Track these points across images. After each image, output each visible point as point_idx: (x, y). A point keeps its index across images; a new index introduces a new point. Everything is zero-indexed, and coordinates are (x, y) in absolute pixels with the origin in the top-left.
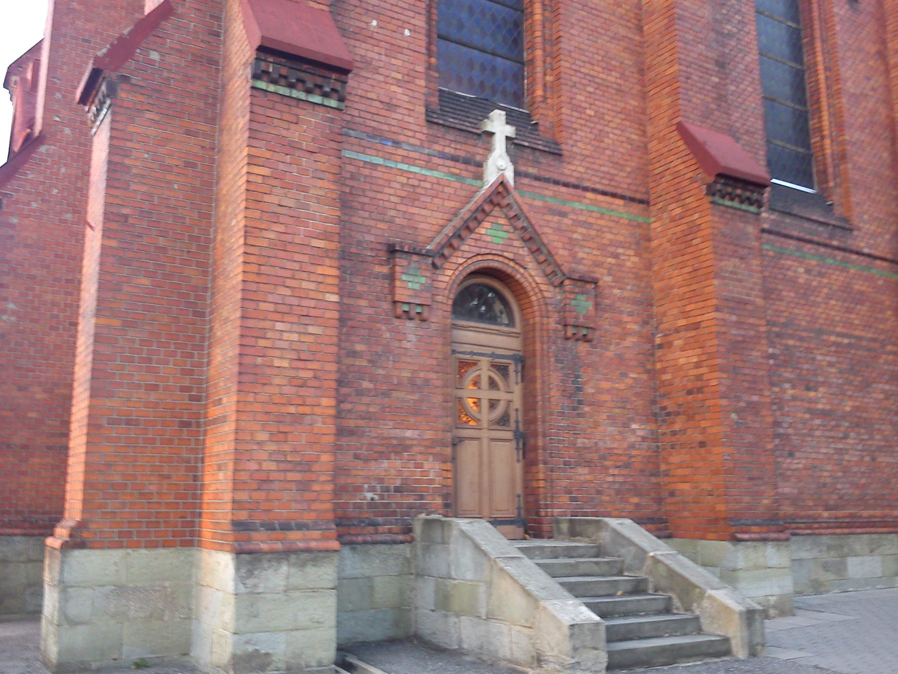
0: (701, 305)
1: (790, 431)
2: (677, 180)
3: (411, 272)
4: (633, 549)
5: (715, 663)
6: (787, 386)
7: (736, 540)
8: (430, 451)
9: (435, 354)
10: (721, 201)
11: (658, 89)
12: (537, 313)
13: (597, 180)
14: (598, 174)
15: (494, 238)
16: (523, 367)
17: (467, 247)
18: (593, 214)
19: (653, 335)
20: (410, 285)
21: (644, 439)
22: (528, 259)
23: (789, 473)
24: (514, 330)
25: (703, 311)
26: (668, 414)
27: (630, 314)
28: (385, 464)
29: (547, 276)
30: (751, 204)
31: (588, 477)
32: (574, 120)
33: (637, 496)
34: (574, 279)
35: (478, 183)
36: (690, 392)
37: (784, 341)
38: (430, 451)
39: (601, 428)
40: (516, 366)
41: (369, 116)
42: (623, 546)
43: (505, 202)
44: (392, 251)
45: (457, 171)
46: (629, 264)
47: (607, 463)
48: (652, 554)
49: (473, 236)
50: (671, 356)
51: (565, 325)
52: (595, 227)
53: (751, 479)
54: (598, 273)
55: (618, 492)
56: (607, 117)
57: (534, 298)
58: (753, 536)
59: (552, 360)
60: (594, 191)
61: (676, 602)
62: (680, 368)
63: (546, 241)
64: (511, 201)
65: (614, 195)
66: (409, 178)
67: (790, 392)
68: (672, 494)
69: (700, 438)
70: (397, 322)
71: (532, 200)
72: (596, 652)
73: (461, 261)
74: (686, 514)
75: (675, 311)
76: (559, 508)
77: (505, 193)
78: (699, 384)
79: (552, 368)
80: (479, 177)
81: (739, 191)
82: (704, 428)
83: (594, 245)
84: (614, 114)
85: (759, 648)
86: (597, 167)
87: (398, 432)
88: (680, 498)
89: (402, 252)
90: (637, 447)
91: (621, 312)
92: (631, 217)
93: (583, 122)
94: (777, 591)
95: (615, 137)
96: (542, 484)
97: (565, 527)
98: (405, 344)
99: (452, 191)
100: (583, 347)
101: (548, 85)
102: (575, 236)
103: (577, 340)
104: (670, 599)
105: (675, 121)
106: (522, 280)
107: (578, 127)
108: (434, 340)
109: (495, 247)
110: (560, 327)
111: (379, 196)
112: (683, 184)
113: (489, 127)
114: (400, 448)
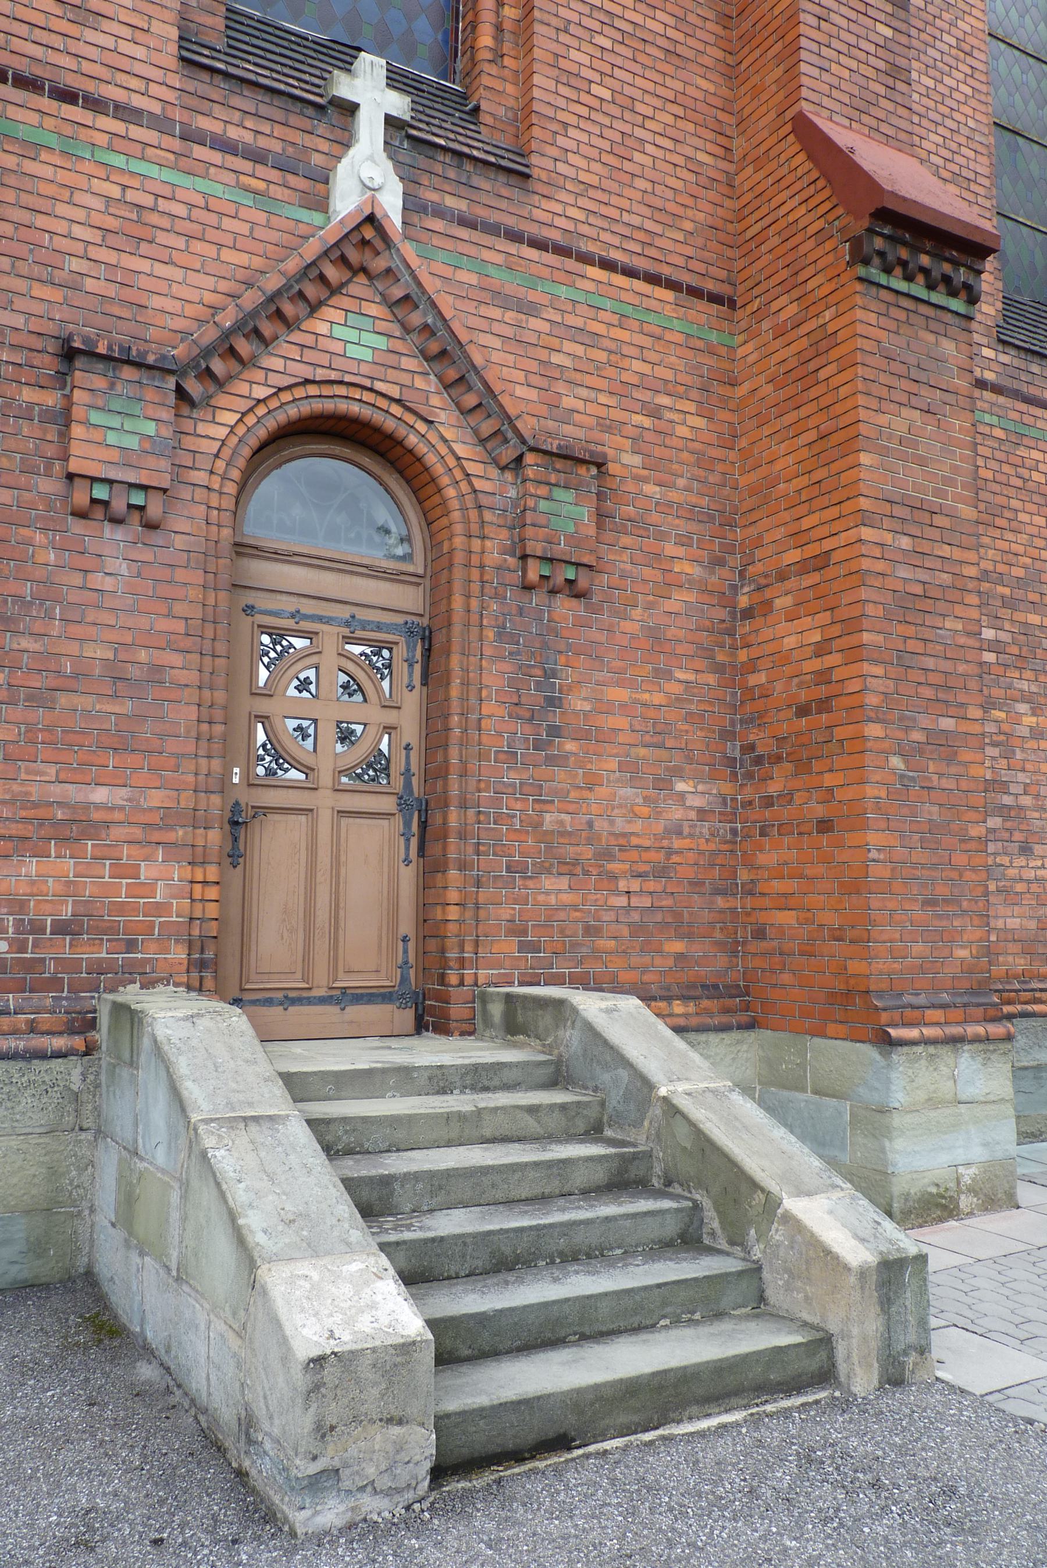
0: (834, 512)
1: (1026, 801)
2: (789, 244)
3: (115, 405)
4: (624, 1074)
5: (786, 1413)
6: (1023, 708)
7: (887, 1042)
8: (156, 836)
9: (179, 609)
10: (883, 279)
11: (757, 53)
12: (458, 528)
13: (616, 241)
14: (616, 228)
15: (352, 342)
16: (428, 652)
17: (283, 363)
18: (602, 315)
19: (734, 588)
20: (112, 438)
21: (703, 814)
22: (435, 401)
23: (1020, 887)
24: (411, 569)
25: (836, 527)
26: (758, 761)
27: (683, 541)
28: (32, 866)
29: (482, 441)
30: (953, 293)
31: (567, 898)
32: (561, 103)
33: (680, 937)
34: (546, 453)
35: (317, 218)
36: (803, 711)
37: (1019, 616)
38: (156, 836)
39: (602, 791)
40: (411, 648)
41: (23, 30)
42: (606, 1067)
43: (378, 264)
44: (69, 354)
45: (261, 186)
46: (682, 431)
47: (614, 867)
48: (663, 1091)
49: (296, 337)
50: (767, 633)
51: (524, 557)
52: (606, 343)
53: (928, 903)
54: (610, 445)
55: (636, 930)
56: (639, 107)
57: (451, 492)
58: (929, 1032)
59: (490, 634)
60: (608, 265)
61: (712, 1220)
62: (783, 658)
63: (478, 359)
64: (396, 263)
65: (653, 279)
66: (125, 187)
67: (1030, 720)
68: (760, 934)
69: (820, 811)
70: (77, 527)
71: (449, 271)
72: (396, 1430)
73: (261, 392)
74: (786, 978)
75: (780, 533)
76: (493, 970)
77: (379, 244)
78: (823, 691)
79: (488, 651)
80: (321, 204)
81: (925, 260)
82: (830, 790)
83: (604, 384)
84: (658, 103)
85: (912, 1358)
86: (614, 213)
87: (73, 793)
88: (775, 943)
89: (92, 355)
90: (686, 831)
91: (661, 537)
92: (693, 330)
93: (584, 111)
94: (978, 1153)
95: (659, 153)
96: (453, 913)
97: (496, 1010)
98: (97, 580)
99: (244, 229)
100: (564, 608)
101: (507, 25)
102: (556, 359)
103: (553, 592)
104: (697, 1207)
105: (789, 114)
106: (422, 449)
107: (572, 120)
108: (180, 575)
109: (353, 367)
110: (511, 561)
111: (40, 221)
112: (803, 249)
113: (344, 87)
114: (76, 829)
